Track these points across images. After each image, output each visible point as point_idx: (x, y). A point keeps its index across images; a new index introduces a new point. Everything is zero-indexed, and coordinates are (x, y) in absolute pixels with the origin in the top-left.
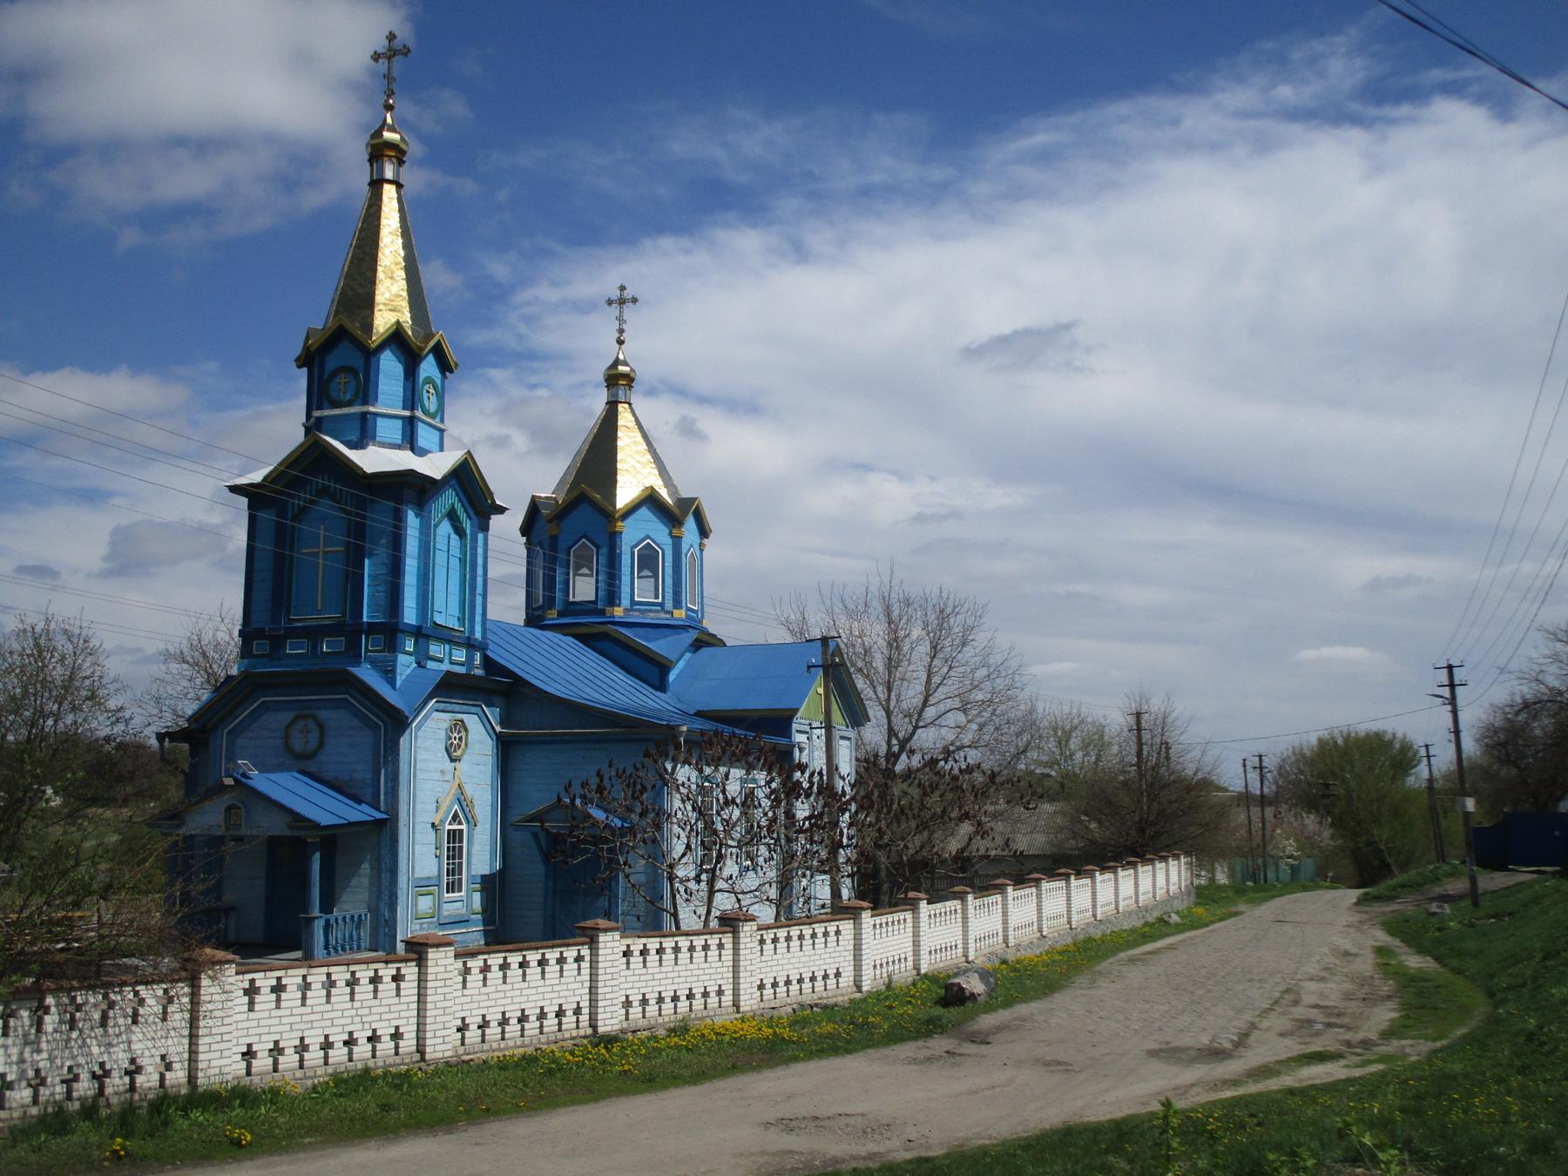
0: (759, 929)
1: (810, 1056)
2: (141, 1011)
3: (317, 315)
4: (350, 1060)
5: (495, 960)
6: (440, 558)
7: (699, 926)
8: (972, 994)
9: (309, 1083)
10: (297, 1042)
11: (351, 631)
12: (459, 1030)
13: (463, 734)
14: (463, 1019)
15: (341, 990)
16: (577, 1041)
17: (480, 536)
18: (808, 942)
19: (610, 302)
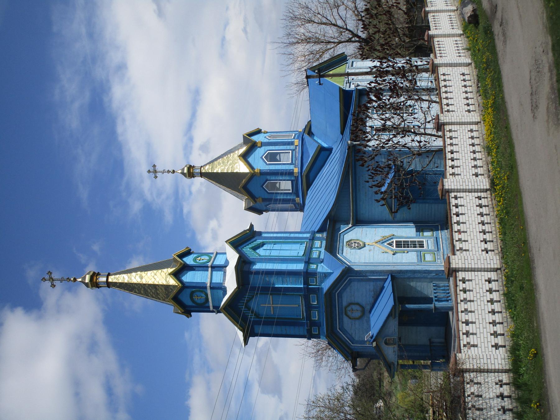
0: (442, 113)
1: (501, 91)
2: (477, 394)
3: (169, 309)
4: (500, 301)
5: (456, 227)
6: (274, 253)
7: (440, 139)
8: (473, 11)
9: (509, 320)
10: (491, 325)
11: (308, 292)
12: (487, 253)
13: (353, 241)
14: (482, 251)
15: (469, 306)
16: (493, 198)
17: (264, 235)
18: (448, 89)
19: (156, 177)
